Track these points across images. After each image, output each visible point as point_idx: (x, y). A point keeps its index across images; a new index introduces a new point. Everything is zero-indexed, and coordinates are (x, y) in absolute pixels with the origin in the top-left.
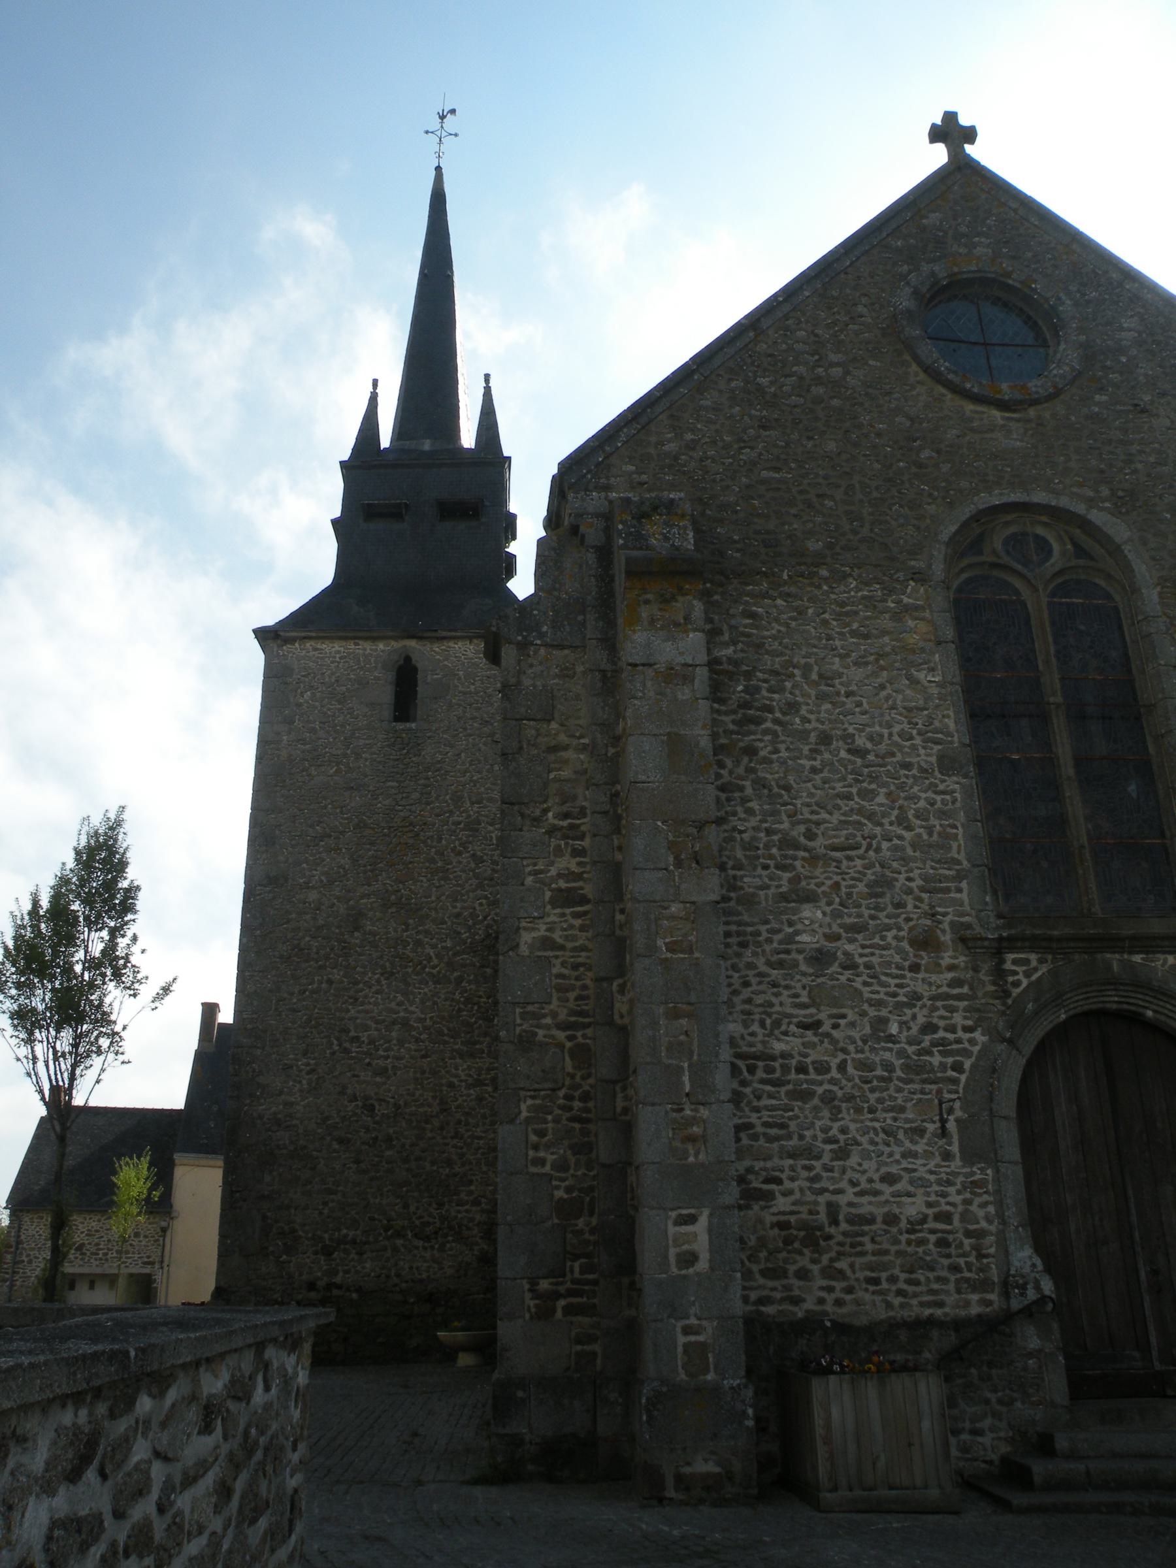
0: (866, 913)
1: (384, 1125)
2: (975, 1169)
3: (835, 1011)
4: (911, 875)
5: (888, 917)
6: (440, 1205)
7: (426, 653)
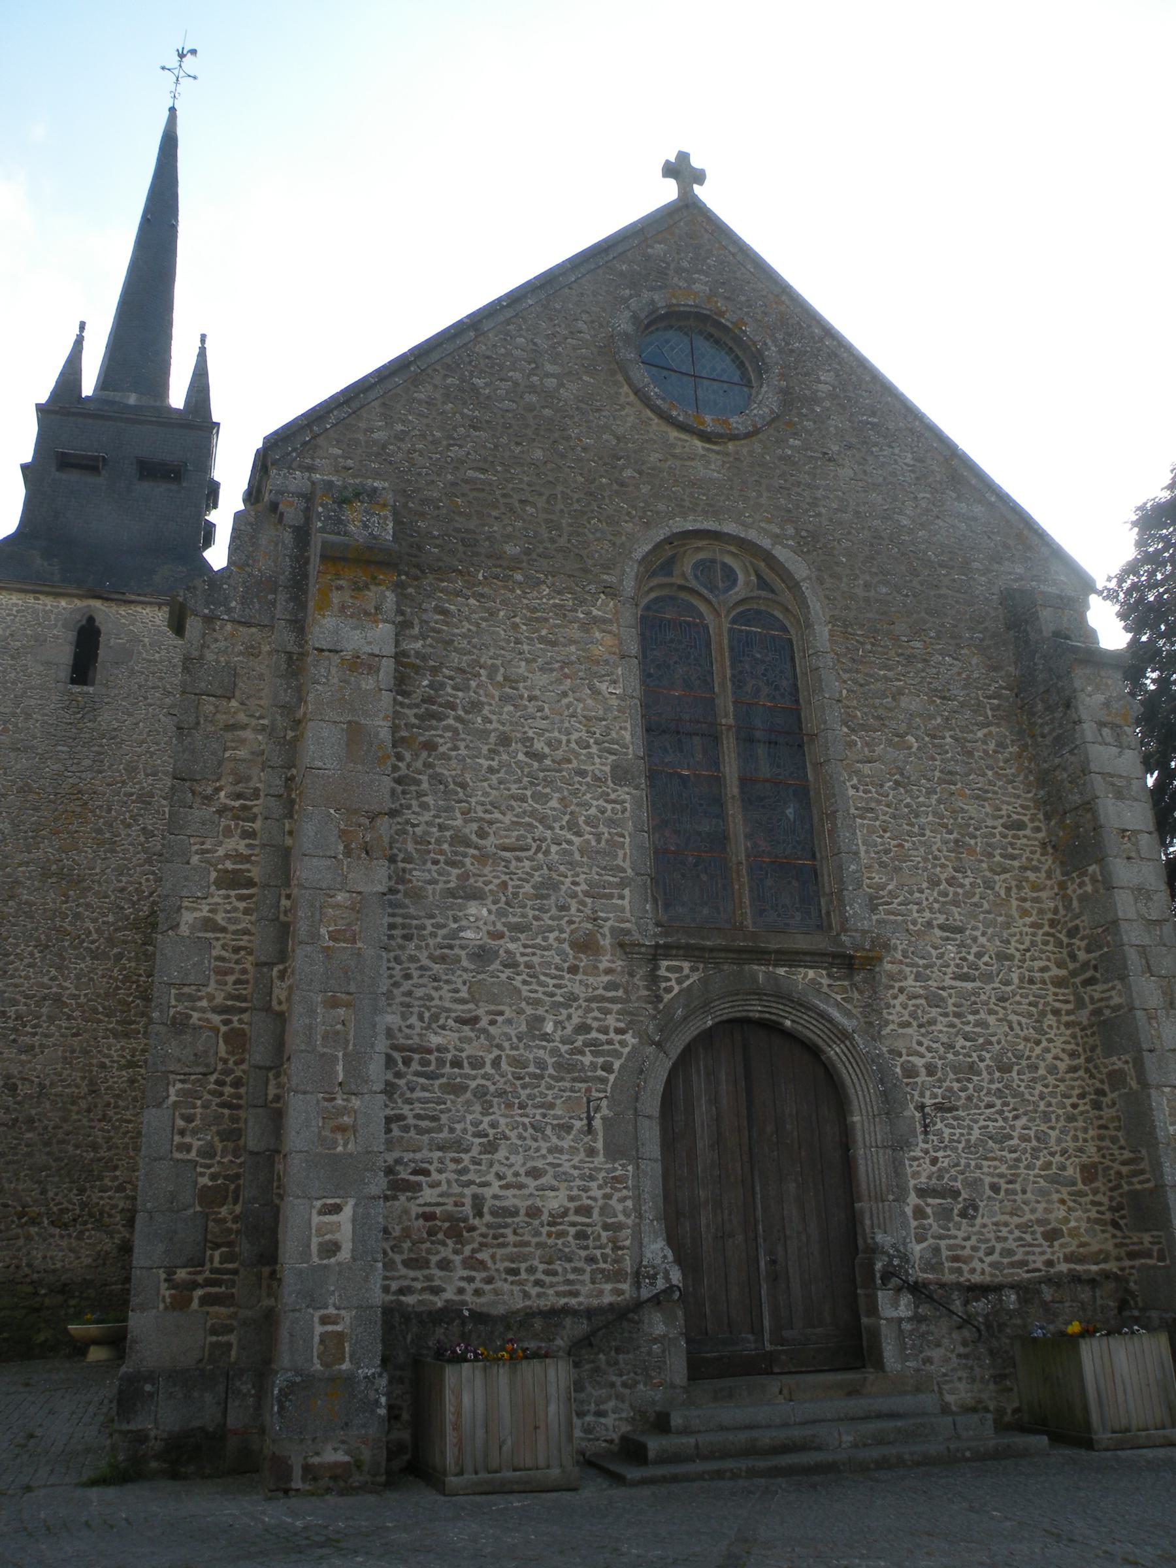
0: (531, 913)
1: (27, 1106)
2: (616, 1165)
3: (493, 1008)
4: (577, 879)
5: (551, 918)
6: (82, 1191)
7: (109, 615)
